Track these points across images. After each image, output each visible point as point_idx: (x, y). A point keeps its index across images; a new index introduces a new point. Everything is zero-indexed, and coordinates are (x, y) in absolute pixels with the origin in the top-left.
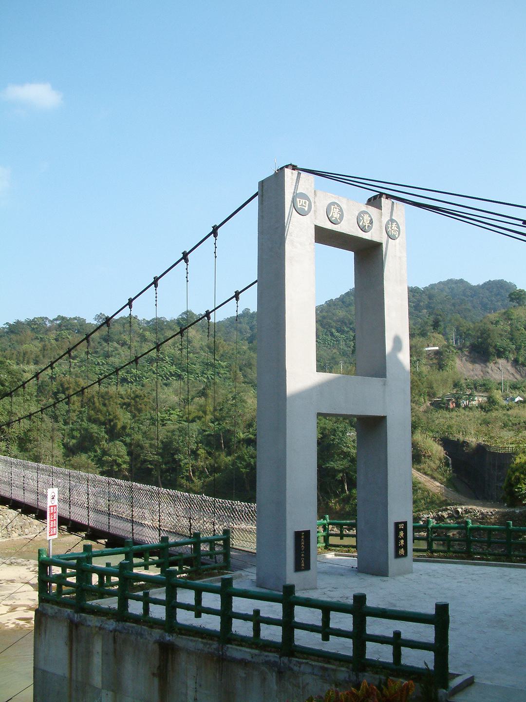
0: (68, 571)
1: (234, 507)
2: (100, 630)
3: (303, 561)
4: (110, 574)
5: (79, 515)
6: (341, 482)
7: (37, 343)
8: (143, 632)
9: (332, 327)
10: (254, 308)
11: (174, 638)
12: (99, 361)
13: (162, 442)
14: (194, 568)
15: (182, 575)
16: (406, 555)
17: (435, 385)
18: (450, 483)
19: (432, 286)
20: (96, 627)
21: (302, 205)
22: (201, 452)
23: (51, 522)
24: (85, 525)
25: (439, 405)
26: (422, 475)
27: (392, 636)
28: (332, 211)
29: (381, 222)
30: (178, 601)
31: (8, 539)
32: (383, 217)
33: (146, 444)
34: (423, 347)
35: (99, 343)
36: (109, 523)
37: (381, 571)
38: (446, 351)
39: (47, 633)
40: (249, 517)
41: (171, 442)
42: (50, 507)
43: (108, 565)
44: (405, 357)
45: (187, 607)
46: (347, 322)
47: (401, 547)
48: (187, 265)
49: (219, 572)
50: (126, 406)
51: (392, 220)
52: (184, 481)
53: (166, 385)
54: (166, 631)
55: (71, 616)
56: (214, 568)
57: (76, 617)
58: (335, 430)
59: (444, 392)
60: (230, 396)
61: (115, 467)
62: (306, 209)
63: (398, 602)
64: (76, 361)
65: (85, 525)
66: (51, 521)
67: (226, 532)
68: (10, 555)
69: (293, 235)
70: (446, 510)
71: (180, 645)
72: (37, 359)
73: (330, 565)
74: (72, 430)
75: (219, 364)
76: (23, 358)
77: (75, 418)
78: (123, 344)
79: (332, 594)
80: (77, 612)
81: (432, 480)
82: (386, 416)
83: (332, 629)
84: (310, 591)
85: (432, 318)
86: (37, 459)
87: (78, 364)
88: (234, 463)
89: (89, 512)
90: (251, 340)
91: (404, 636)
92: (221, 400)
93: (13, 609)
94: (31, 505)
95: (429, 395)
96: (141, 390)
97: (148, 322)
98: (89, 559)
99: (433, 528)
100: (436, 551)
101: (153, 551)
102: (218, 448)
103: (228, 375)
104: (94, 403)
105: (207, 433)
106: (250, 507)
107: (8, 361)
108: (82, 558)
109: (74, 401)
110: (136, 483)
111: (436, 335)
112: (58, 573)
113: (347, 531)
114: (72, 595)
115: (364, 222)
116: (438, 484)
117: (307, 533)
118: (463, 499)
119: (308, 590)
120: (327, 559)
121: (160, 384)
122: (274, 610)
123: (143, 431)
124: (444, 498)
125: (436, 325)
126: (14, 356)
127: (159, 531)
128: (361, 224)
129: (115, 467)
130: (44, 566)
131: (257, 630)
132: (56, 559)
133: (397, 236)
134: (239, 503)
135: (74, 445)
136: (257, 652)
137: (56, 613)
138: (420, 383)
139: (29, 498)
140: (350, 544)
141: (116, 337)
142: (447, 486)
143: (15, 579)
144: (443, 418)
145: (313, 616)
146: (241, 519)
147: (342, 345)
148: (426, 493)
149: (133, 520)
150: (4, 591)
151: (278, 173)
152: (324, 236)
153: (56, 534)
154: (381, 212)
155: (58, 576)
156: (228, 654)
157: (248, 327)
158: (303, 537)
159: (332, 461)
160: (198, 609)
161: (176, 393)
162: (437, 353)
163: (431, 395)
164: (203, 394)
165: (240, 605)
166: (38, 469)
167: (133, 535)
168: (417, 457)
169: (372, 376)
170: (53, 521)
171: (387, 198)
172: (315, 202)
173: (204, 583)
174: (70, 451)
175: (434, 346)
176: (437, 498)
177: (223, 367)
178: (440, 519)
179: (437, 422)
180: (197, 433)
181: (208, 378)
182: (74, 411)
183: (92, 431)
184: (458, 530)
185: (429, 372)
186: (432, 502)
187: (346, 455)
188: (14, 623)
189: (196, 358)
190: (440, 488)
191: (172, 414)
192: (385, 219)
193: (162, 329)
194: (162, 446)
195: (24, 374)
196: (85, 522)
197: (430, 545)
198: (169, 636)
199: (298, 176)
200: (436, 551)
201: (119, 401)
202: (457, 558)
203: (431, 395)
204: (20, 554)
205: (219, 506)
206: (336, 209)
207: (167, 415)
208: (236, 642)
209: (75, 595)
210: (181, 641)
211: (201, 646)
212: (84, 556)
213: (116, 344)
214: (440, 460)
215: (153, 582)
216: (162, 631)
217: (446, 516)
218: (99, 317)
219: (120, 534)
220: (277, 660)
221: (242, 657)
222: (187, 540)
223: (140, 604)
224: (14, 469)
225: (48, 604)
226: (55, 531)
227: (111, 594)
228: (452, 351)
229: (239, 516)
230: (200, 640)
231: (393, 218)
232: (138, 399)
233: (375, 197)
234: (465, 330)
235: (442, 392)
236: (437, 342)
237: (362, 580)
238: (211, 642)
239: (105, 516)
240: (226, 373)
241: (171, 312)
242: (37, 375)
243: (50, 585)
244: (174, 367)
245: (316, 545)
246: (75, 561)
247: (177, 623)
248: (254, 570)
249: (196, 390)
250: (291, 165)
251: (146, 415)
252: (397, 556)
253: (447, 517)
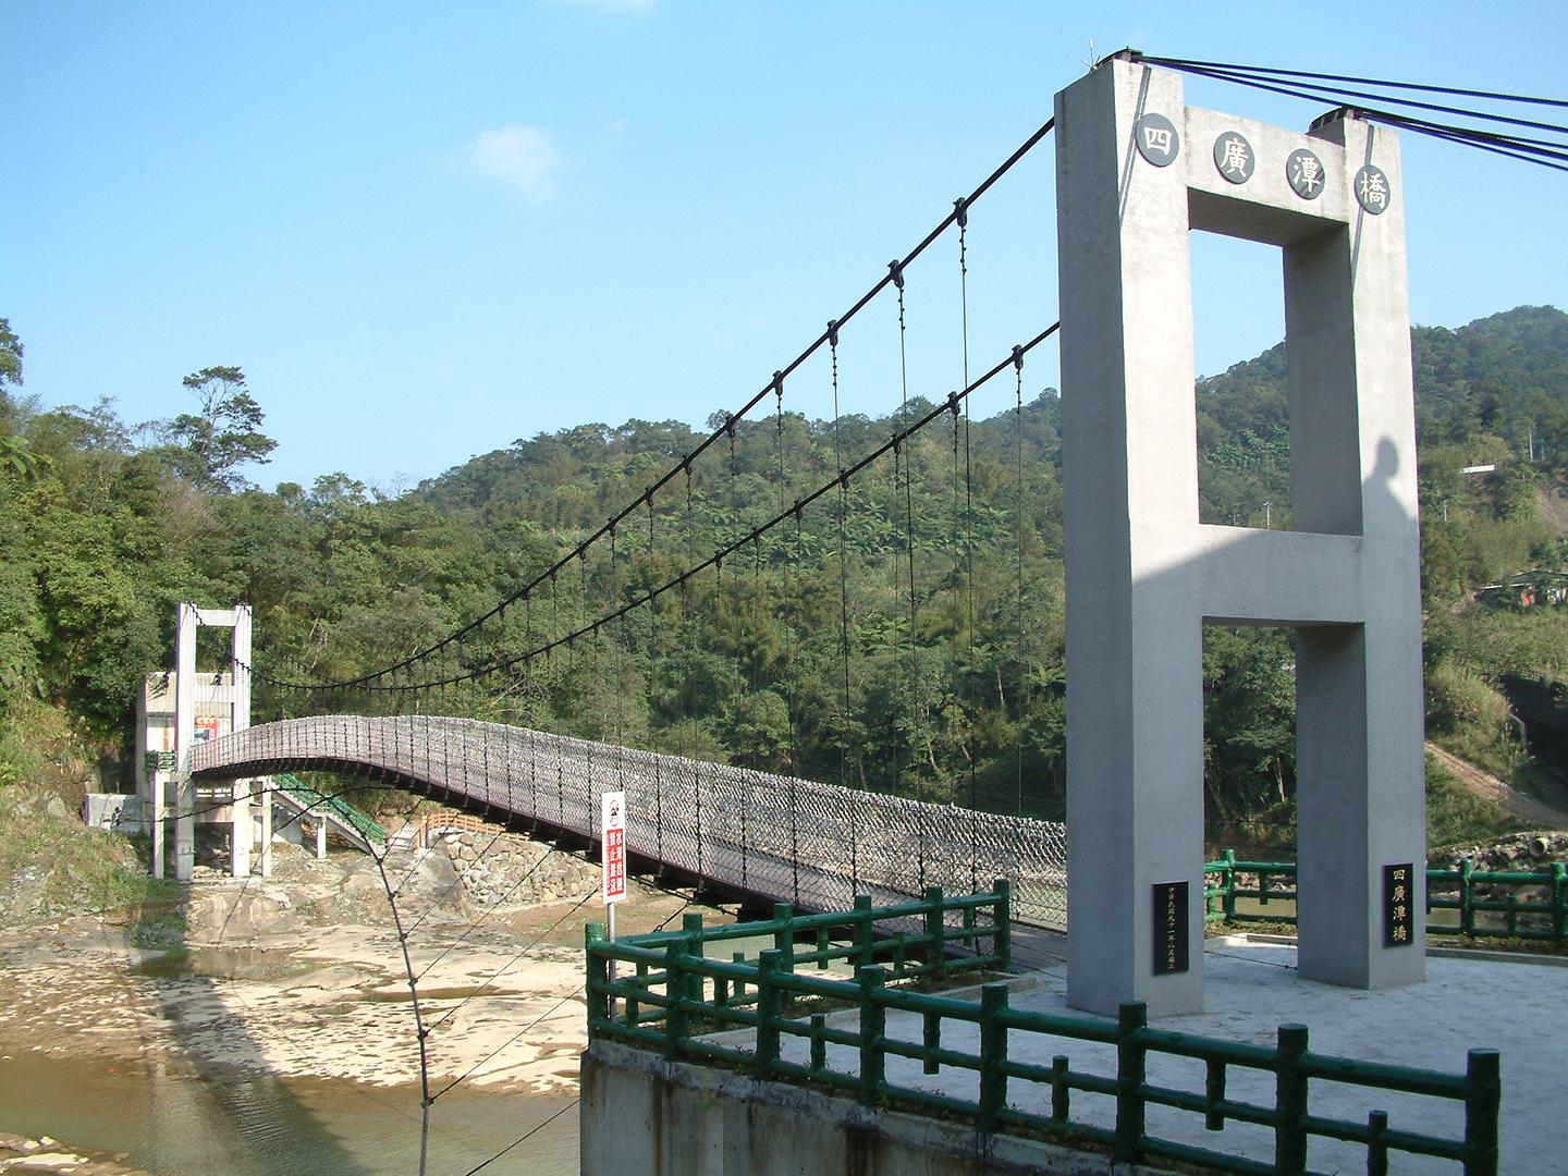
0: (651, 971)
1: (1020, 831)
2: (718, 1097)
3: (1171, 951)
4: (741, 980)
5: (679, 852)
6: (1270, 776)
7: (585, 480)
8: (810, 1103)
9: (1245, 425)
10: (1054, 380)
11: (878, 1117)
12: (723, 516)
13: (866, 692)
14: (930, 966)
15: (902, 981)
16: (1409, 939)
17: (1486, 554)
18: (1522, 780)
19: (1478, 325)
20: (711, 1090)
21: (1156, 142)
22: (954, 713)
23: (613, 865)
24: (691, 874)
25: (1494, 601)
26: (1457, 760)
27: (1366, 1122)
28: (1227, 153)
29: (1343, 174)
30: (887, 1036)
31: (534, 906)
32: (1347, 161)
33: (831, 696)
34: (1458, 466)
35: (721, 476)
36: (745, 868)
37: (1351, 976)
38: (1513, 475)
39: (608, 1102)
40: (1054, 853)
41: (886, 691)
42: (609, 832)
43: (738, 957)
44: (1405, 488)
45: (908, 1051)
46: (1280, 413)
47: (1398, 923)
48: (902, 291)
49: (984, 975)
50: (785, 611)
51: (1369, 169)
52: (914, 777)
53: (872, 564)
54: (861, 1103)
55: (658, 1067)
56: (974, 967)
57: (669, 1070)
58: (1255, 660)
59: (1507, 569)
60: (1015, 585)
61: (762, 748)
62: (1166, 150)
63: (1388, 1046)
64: (672, 518)
65: (693, 873)
66: (611, 863)
67: (1001, 886)
68: (539, 938)
69: (1137, 213)
70: (1513, 840)
71: (890, 1132)
72: (587, 517)
73: (1231, 960)
74: (668, 668)
75: (991, 514)
76: (557, 514)
77: (674, 643)
78: (776, 477)
79: (1238, 1026)
80: (669, 1058)
81: (1480, 772)
82: (1363, 623)
83: (1229, 1103)
84: (1189, 1018)
85: (1477, 399)
86: (592, 733)
87: (676, 524)
88: (1026, 736)
89: (700, 845)
90: (1058, 460)
91: (1393, 1124)
92: (995, 596)
93: (548, 1052)
94: (576, 831)
95: (1472, 577)
96: (818, 577)
97: (828, 426)
98: (694, 946)
99: (1473, 880)
100: (1480, 933)
101: (837, 928)
102: (991, 703)
103: (1011, 539)
104: (714, 609)
105: (963, 669)
106: (1055, 830)
107: (525, 523)
108: (679, 943)
109: (670, 606)
110: (803, 780)
111: (1488, 438)
112: (627, 975)
113: (1284, 888)
114: (659, 1023)
115: (1302, 176)
116: (1494, 781)
117: (1181, 890)
118: (1552, 815)
119: (1183, 1015)
120: (1230, 947)
121: (859, 562)
122: (1098, 1058)
123: (824, 667)
124: (1508, 814)
125: (1488, 415)
126: (538, 512)
127: (854, 885)
128: (1296, 180)
129: (762, 748)
130: (598, 960)
131: (1061, 1103)
132: (625, 946)
133: (1382, 205)
134: (1032, 823)
135: (672, 702)
136: (1060, 1150)
137: (625, 1060)
138: (1451, 551)
139: (571, 817)
140: (1283, 914)
141: (758, 462)
142: (1515, 786)
143: (552, 989)
144: (1507, 630)
145: (1187, 1074)
146: (1037, 859)
147: (1270, 466)
148: (1465, 801)
149: (795, 862)
150: (528, 1015)
151: (1097, 71)
152: (1209, 212)
153: (622, 892)
154: (1344, 151)
155: (629, 981)
156: (997, 1154)
157: (1054, 430)
158: (1172, 897)
159: (1247, 728)
160: (932, 1056)
161: (894, 581)
162: (1490, 478)
163: (1477, 576)
164: (953, 582)
165: (1024, 1046)
166: (590, 753)
167: (796, 895)
168: (1441, 719)
169: (1330, 532)
170: (616, 862)
171: (1357, 117)
172: (1186, 135)
173: (951, 999)
174: (664, 714)
175: (1484, 463)
176: (1492, 814)
177: (998, 522)
178: (1499, 860)
179: (1491, 638)
180: (942, 669)
181: (965, 547)
182: (671, 627)
183: (712, 669)
184: (1542, 887)
185: (1471, 523)
186: (1481, 823)
187: (1280, 715)
189: (937, 504)
190: (1497, 792)
191: (888, 628)
192: (1353, 167)
193: (862, 441)
194: (864, 700)
195: (560, 549)
196: (693, 866)
197: (1467, 918)
198: (868, 1114)
199: (1144, 76)
200: (1480, 933)
201: (772, 602)
202: (1530, 949)
203: (1477, 576)
204: (563, 939)
205: (987, 827)
206: (1237, 147)
207: (875, 631)
208: (1015, 1130)
209: (664, 1021)
210: (894, 1124)
211: (938, 1136)
212: (684, 937)
213: (758, 478)
214: (1499, 725)
215: (835, 995)
216: (853, 1102)
217: (1512, 855)
218: (712, 421)
219: (769, 892)
220: (1105, 1169)
221: (1028, 1162)
222: (917, 903)
223: (806, 1042)
224: (539, 755)
225: (607, 1042)
226: (619, 885)
227: (744, 1021)
228: (1528, 475)
229: (1031, 849)
230: (935, 1122)
231: (1372, 163)
232: (810, 597)
233: (1328, 117)
234: (1558, 426)
235: (1502, 570)
236: (1490, 454)
237: (1306, 996)
238: (961, 1127)
239: (735, 853)
240: (1006, 536)
241: (880, 404)
242: (581, 549)
243: (613, 1001)
244: (889, 524)
245: (1203, 916)
246: (664, 950)
247: (886, 1085)
248: (1062, 970)
249: (937, 575)
250: (1127, 50)
251: (829, 632)
252: (1390, 942)
253: (1516, 858)
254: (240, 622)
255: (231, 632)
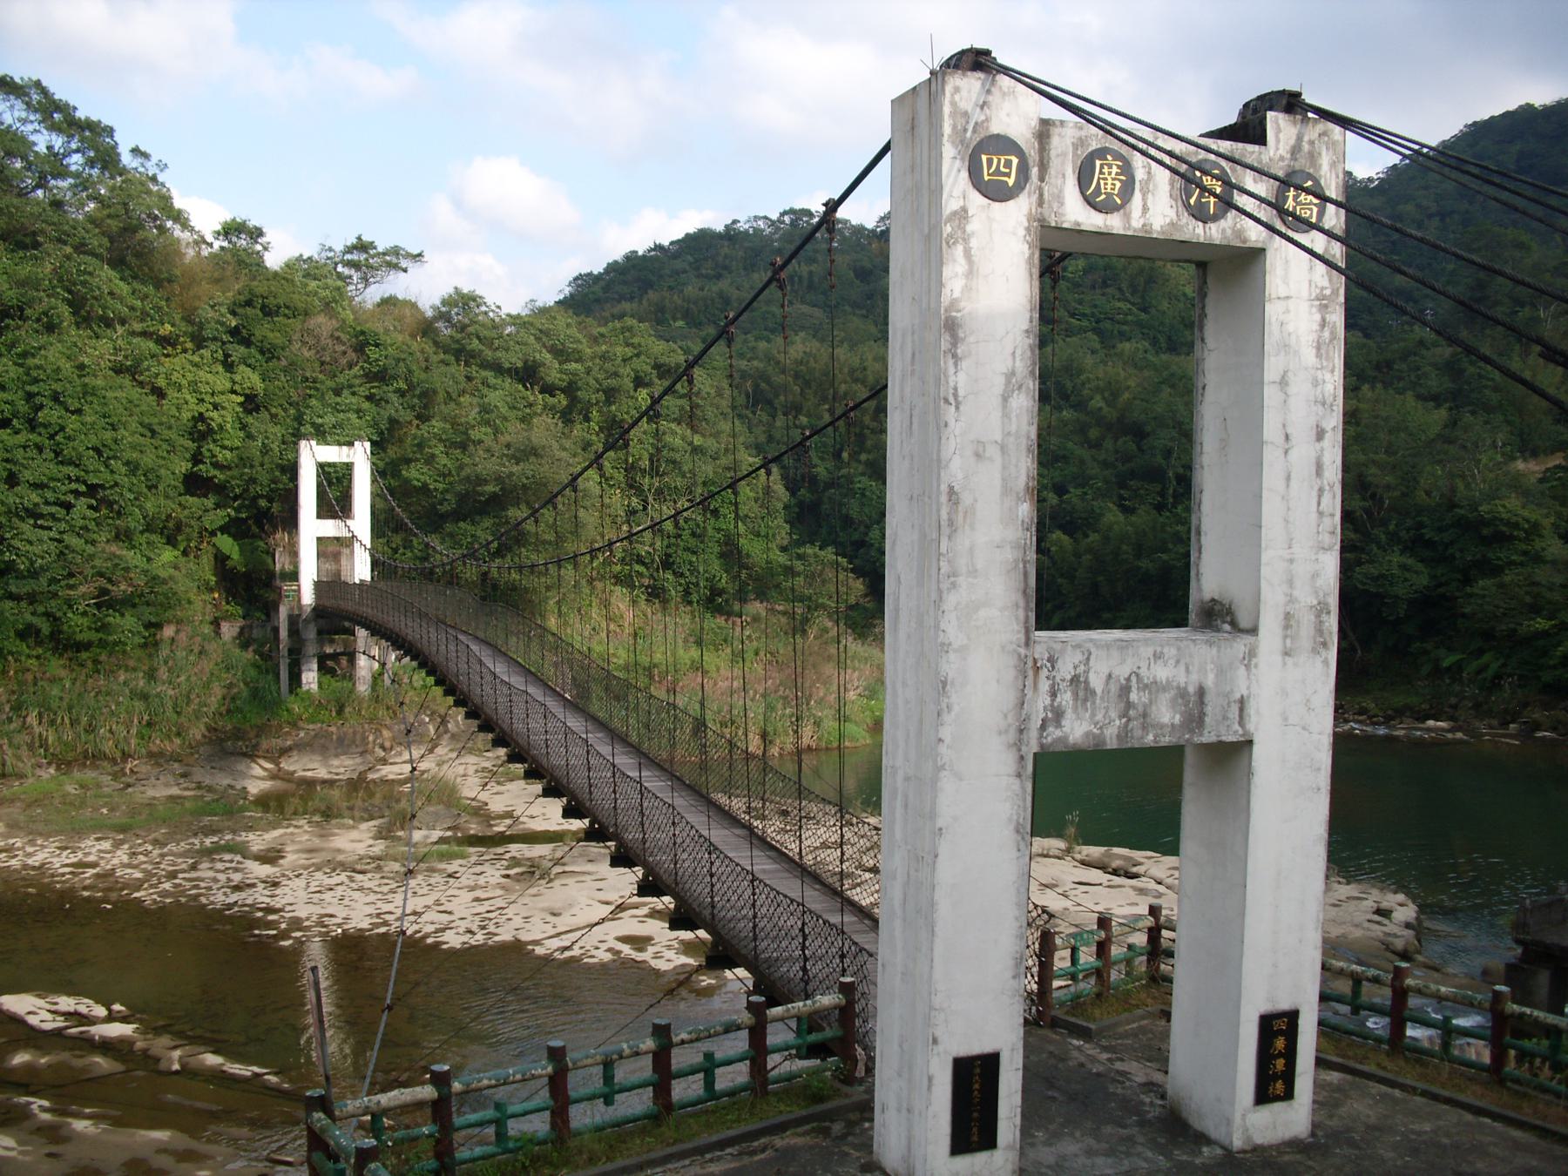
47: (1275, 1078)
158: (978, 1070)
188: (609, 950)
254: (359, 457)
255: (349, 467)
